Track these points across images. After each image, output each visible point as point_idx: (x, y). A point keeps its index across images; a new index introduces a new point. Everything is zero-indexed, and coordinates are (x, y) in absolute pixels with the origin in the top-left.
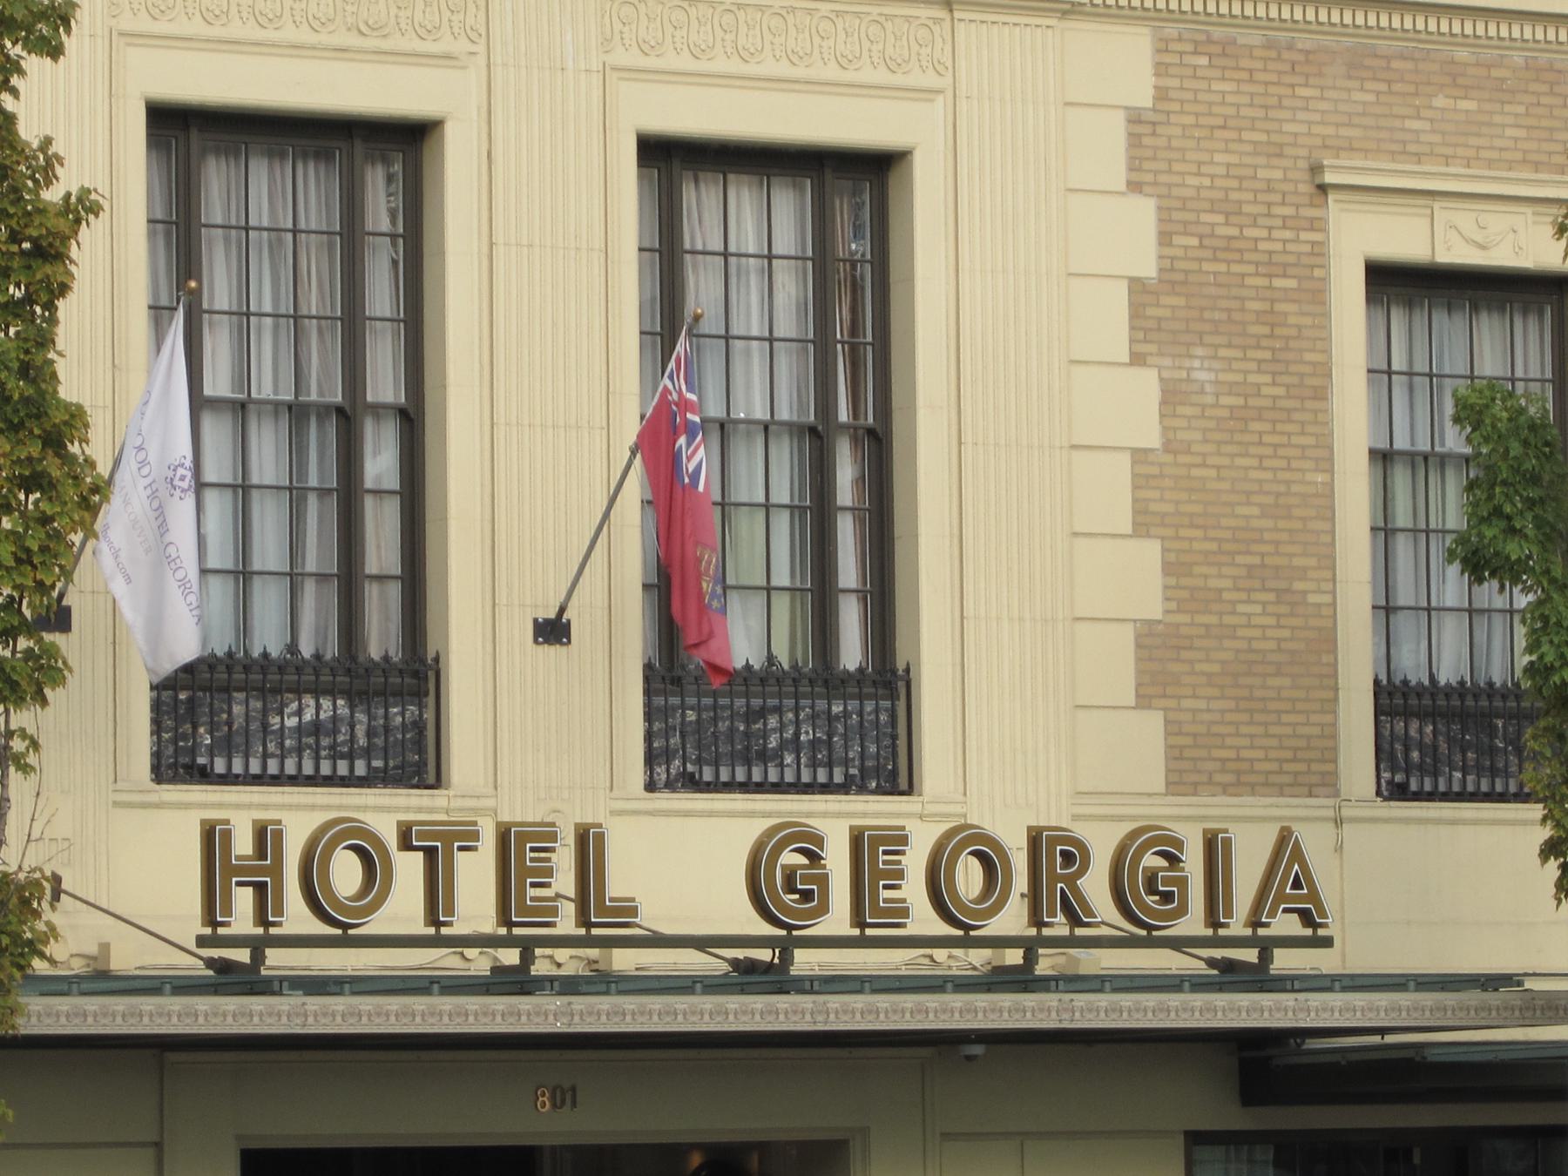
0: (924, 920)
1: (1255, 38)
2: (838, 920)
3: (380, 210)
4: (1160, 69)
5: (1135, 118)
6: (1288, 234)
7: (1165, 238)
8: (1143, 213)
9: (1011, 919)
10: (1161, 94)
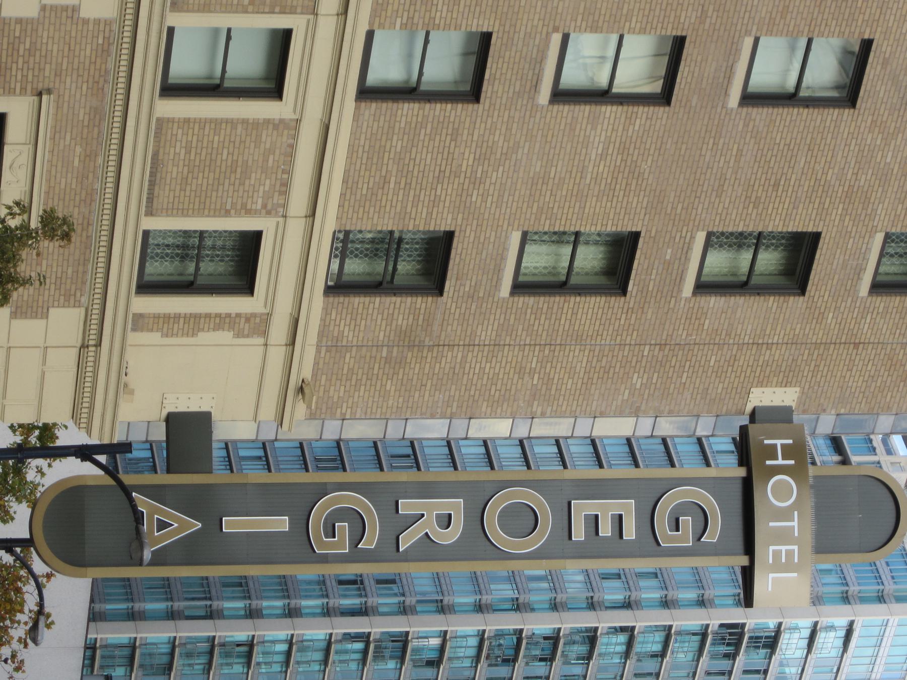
1: (110, 65)
4: (97, 22)
5: (75, 9)
6: (19, 77)
7: (19, 21)
8: (32, 12)
10: (86, 22)
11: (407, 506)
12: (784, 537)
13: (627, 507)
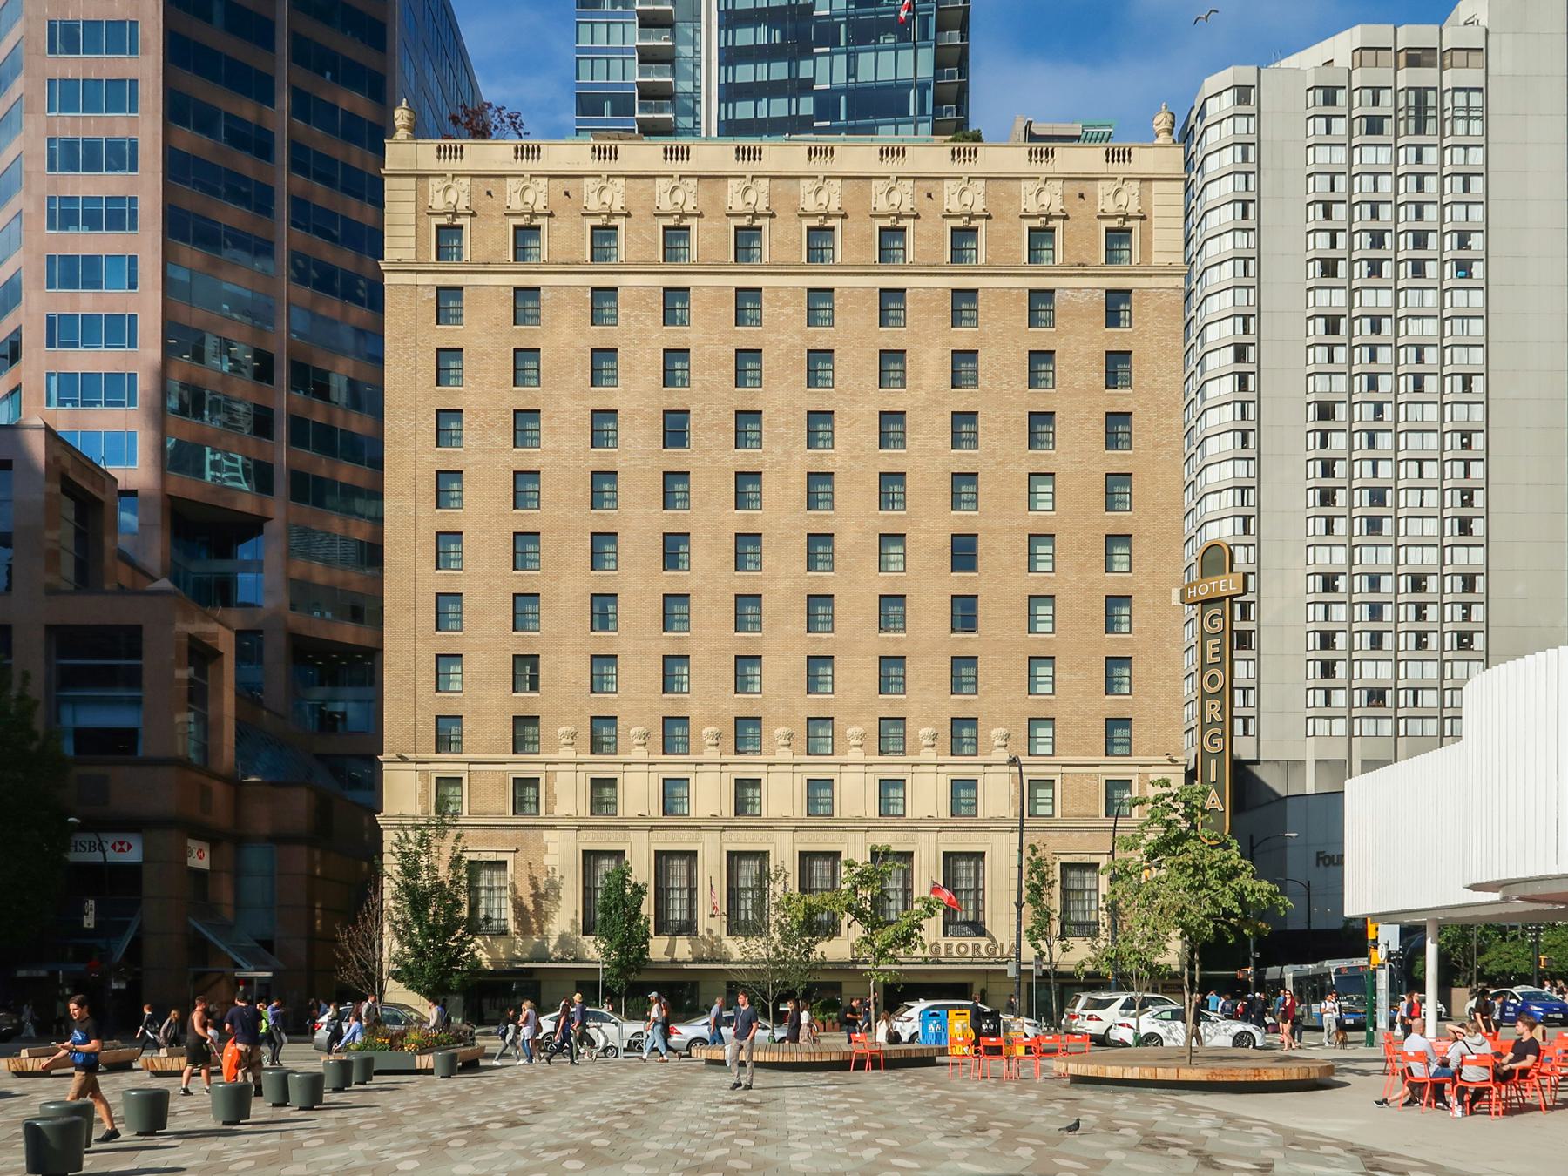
0: (955, 954)
2: (943, 954)
3: (981, 864)
9: (970, 954)
11: (1208, 720)
12: (1218, 586)
13: (1210, 643)
